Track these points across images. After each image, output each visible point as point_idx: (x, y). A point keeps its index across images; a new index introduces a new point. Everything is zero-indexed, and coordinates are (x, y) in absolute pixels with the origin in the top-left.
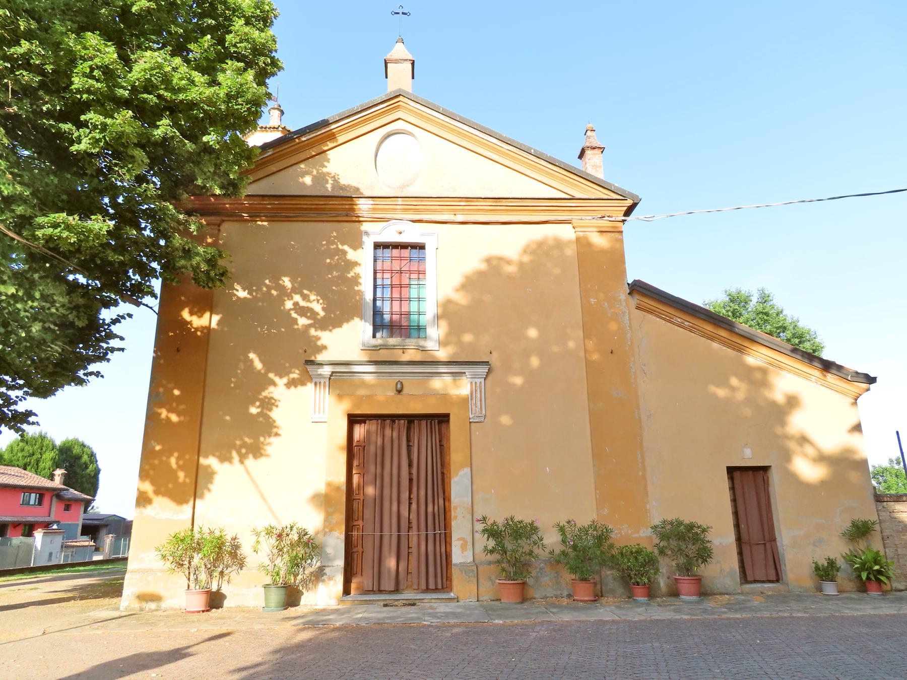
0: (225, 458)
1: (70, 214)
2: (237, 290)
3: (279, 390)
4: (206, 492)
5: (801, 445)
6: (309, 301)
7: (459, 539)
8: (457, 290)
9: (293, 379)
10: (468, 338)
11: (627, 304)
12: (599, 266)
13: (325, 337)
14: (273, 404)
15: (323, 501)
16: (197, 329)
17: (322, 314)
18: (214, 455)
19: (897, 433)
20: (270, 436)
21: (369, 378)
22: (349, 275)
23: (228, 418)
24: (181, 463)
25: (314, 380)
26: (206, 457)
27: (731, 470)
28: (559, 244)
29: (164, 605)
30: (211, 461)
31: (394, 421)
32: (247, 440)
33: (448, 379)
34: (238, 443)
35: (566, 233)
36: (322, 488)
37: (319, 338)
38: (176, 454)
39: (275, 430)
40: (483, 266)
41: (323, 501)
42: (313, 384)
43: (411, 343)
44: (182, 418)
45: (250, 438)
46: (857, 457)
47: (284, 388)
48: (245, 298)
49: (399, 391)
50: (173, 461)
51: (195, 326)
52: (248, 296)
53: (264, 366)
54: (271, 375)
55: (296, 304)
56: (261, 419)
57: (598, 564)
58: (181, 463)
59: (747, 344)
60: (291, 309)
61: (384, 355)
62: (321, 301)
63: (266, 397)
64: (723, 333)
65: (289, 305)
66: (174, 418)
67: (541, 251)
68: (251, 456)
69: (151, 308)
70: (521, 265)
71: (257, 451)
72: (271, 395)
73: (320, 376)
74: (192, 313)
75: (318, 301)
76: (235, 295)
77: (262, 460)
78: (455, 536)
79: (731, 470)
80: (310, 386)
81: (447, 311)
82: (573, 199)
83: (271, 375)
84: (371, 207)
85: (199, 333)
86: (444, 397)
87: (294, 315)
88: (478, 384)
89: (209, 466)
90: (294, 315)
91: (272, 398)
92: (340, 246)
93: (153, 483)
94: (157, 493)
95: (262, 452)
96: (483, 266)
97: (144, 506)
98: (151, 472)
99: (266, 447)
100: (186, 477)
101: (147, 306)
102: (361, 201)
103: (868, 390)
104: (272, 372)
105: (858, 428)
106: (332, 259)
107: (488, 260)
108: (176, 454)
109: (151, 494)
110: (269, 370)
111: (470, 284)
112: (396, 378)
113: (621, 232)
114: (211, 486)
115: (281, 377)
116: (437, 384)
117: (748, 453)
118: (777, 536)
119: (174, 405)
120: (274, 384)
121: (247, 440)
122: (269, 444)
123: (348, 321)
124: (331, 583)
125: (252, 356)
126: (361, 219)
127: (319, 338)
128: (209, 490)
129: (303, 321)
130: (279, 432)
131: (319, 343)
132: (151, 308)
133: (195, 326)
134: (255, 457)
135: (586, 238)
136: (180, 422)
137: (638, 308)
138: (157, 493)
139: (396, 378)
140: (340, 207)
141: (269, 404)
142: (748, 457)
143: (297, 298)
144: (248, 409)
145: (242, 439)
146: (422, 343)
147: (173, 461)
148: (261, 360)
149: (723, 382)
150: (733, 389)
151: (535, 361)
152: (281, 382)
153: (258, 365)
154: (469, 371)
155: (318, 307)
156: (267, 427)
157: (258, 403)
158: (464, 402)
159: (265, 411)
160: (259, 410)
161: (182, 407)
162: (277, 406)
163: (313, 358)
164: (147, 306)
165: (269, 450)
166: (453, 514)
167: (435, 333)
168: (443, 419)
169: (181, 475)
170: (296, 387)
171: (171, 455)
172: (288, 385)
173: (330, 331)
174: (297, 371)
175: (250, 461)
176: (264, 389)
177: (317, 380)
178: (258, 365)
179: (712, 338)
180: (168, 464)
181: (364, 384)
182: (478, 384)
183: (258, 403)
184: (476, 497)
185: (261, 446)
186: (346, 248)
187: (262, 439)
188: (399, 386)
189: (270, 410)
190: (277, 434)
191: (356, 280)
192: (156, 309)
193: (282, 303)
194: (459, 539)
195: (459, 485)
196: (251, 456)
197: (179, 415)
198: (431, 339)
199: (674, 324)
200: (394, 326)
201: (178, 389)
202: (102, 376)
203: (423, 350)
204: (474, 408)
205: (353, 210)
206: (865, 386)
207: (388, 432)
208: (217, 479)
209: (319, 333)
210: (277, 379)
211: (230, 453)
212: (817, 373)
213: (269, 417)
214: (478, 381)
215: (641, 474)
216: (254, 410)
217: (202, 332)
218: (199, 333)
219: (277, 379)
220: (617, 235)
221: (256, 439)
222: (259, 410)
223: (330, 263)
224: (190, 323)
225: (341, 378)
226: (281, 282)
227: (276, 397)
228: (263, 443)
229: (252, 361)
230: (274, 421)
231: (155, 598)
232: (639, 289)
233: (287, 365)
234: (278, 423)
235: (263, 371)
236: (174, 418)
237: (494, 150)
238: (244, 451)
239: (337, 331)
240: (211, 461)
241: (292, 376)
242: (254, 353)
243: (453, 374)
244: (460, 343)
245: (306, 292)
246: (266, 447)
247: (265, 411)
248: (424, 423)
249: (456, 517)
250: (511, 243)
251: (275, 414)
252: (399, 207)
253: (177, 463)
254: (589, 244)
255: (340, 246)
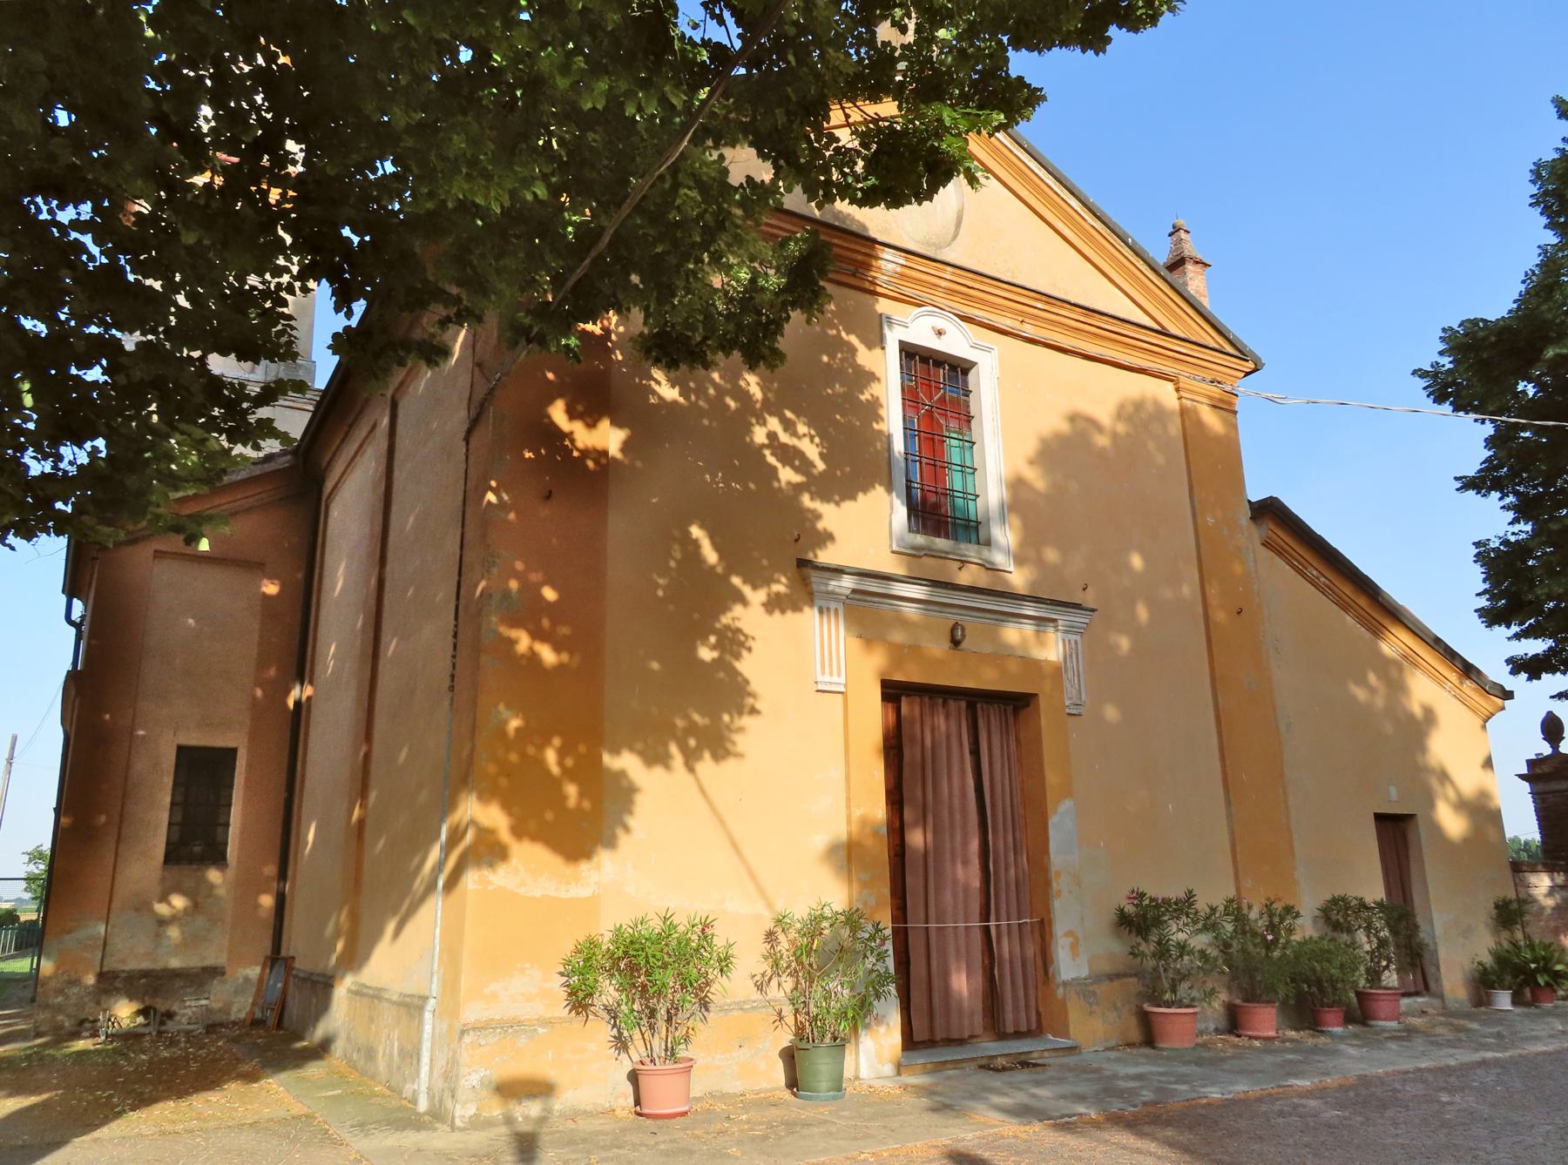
0: (655, 757)
1: (875, 99)
2: (658, 383)
3: (750, 614)
4: (620, 832)
5: (1442, 783)
6: (795, 434)
8: (1031, 463)
9: (778, 594)
10: (1051, 555)
11: (1250, 536)
12: (1209, 458)
13: (831, 516)
14: (742, 644)
15: (847, 855)
16: (585, 453)
17: (821, 466)
18: (631, 749)
19: (15, 739)
20: (740, 714)
21: (910, 610)
22: (863, 398)
23: (655, 666)
24: (569, 762)
25: (818, 602)
26: (616, 751)
27: (1379, 818)
28: (1160, 413)
29: (558, 1104)
30: (626, 762)
32: (697, 717)
33: (1029, 628)
34: (680, 723)
35: (1165, 393)
36: (839, 830)
37: (818, 516)
38: (557, 741)
39: (750, 701)
40: (1064, 427)
41: (847, 855)
42: (816, 610)
43: (970, 551)
44: (565, 657)
45: (703, 715)
46: (1492, 805)
47: (762, 610)
48: (675, 402)
49: (956, 643)
50: (551, 756)
51: (580, 444)
52: (681, 400)
53: (721, 558)
54: (736, 581)
55: (772, 436)
56: (722, 675)
58: (569, 762)
59: (1386, 623)
60: (763, 446)
61: (930, 567)
62: (817, 440)
63: (728, 627)
64: (1363, 602)
65: (760, 435)
66: (548, 655)
67: (1138, 415)
68: (707, 755)
70: (1115, 436)
71: (718, 744)
72: (738, 624)
73: (832, 595)
74: (572, 414)
75: (812, 439)
76: (654, 393)
77: (730, 763)
78: (1060, 928)
79: (1379, 818)
80: (810, 615)
81: (1019, 497)
82: (1164, 333)
83: (736, 581)
84: (899, 269)
85: (590, 464)
86: (1033, 666)
87: (771, 460)
89: (622, 774)
90: (771, 460)
91: (739, 631)
92: (843, 334)
93: (507, 806)
94: (518, 832)
95: (729, 746)
96: (1064, 427)
97: (491, 865)
98: (503, 782)
99: (737, 737)
100: (581, 795)
102: (888, 254)
103: (1503, 708)
104: (737, 574)
105: (1488, 763)
106: (832, 356)
107: (1073, 418)
108: (557, 741)
109: (505, 835)
110: (731, 569)
111: (1052, 453)
112: (952, 617)
113: (1235, 413)
114: (631, 821)
115: (755, 588)
116: (1014, 634)
119: (546, 623)
120: (742, 600)
121: (697, 717)
122: (741, 730)
123: (865, 491)
124: (882, 1029)
125: (696, 531)
126: (879, 289)
127: (818, 516)
128: (627, 829)
129: (787, 475)
130: (758, 706)
131: (820, 525)
133: (580, 444)
134: (717, 757)
135: (1196, 411)
136: (560, 667)
137: (1265, 544)
138: (518, 832)
139: (952, 617)
140: (849, 254)
141: (734, 643)
142: (1393, 804)
143: (774, 423)
144: (694, 650)
145: (687, 717)
146: (985, 553)
147: (551, 756)
148: (716, 547)
149: (1362, 682)
150: (1372, 691)
151: (1142, 613)
152: (757, 597)
153: (711, 556)
154: (1063, 618)
155: (812, 451)
156: (731, 694)
157: (713, 639)
158: (1057, 672)
159: (728, 657)
160: (715, 654)
161: (564, 630)
162: (750, 650)
163: (810, 556)
165: (741, 742)
166: (1054, 885)
167: (1005, 536)
168: (1017, 704)
169: (571, 790)
170: (783, 612)
171: (547, 742)
172: (775, 604)
173: (837, 504)
174: (783, 580)
175: (706, 766)
176: (726, 609)
177: (824, 604)
178: (711, 556)
179: (1345, 607)
180: (541, 763)
181: (903, 622)
183: (713, 639)
185: (726, 733)
186: (853, 339)
187: (726, 718)
189: (738, 656)
190: (754, 711)
191: (873, 410)
193: (748, 430)
195: (1064, 830)
196: (707, 755)
197: (557, 648)
198: (999, 548)
200: (937, 514)
201: (554, 587)
203: (991, 568)
205: (868, 267)
206: (1499, 701)
207: (941, 721)
208: (642, 802)
209: (817, 505)
210: (747, 590)
211: (666, 746)
212: (1453, 677)
213: (737, 673)
216: (706, 654)
217: (596, 462)
218: (590, 464)
219: (747, 590)
220: (1230, 416)
221: (716, 718)
222: (715, 654)
223: (828, 364)
224: (570, 436)
225: (866, 605)
226: (742, 383)
227: (747, 630)
228: (728, 727)
229: (696, 544)
230: (747, 682)
231: (540, 1089)
232: (1271, 512)
233: (765, 562)
234: (754, 686)
235: (719, 570)
236: (548, 655)
237: (1068, 219)
238: (692, 742)
239: (847, 505)
240: (626, 762)
241: (777, 588)
242: (701, 527)
243: (1040, 621)
244: (1040, 563)
245: (789, 414)
246: (737, 737)
247: (728, 657)
248: (952, 704)
250: (1102, 393)
251: (746, 666)
252: (944, 284)
253: (560, 763)
254: (1200, 424)
255: (843, 334)
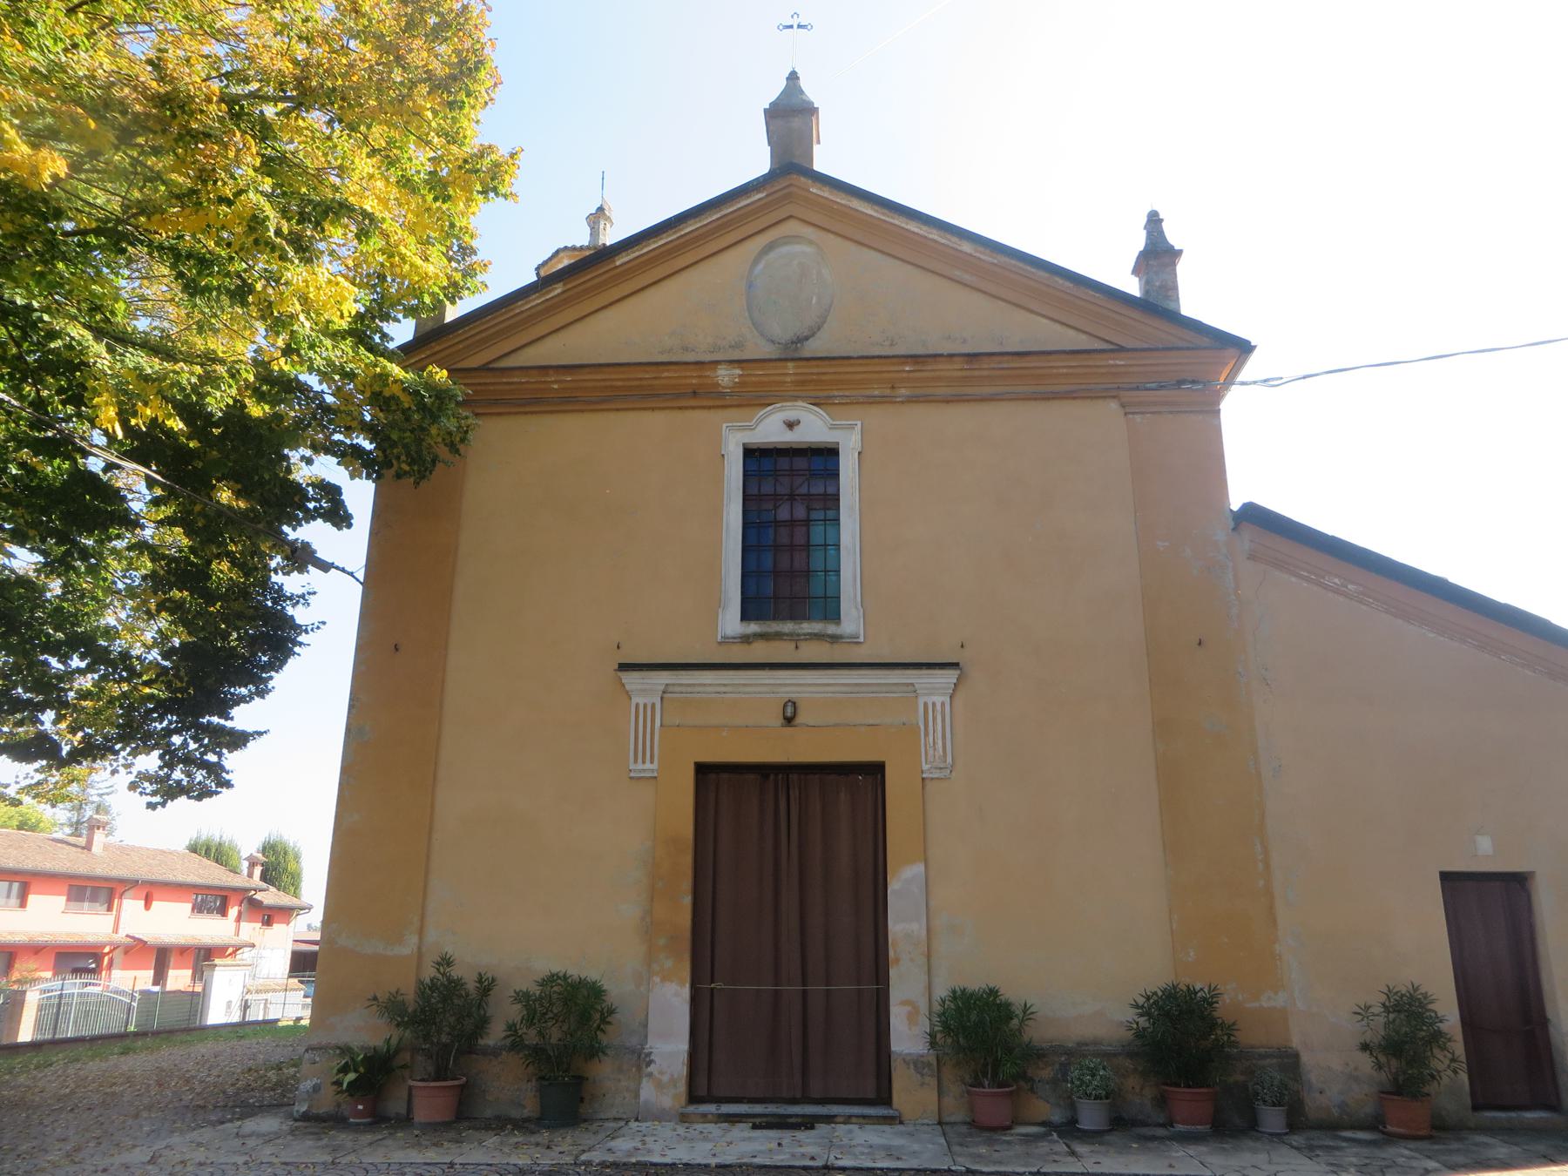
7: (904, 1003)
31: (766, 777)
40: (242, 717)
49: (789, 721)
57: (1190, 1060)
69: (351, 574)
78: (896, 994)
79: (1446, 877)
82: (1121, 349)
88: (939, 707)
101: (343, 570)
117: (1485, 844)
118: (1550, 1014)
132: (351, 574)
164: (343, 570)
182: (939, 707)
184: (942, 930)
188: (789, 711)
192: (361, 575)
194: (904, 1003)
199: (1326, 588)
202: (1154, 221)
204: (931, 752)
214: (938, 699)
215: (1261, 883)
232: (1254, 516)
249: (897, 960)
